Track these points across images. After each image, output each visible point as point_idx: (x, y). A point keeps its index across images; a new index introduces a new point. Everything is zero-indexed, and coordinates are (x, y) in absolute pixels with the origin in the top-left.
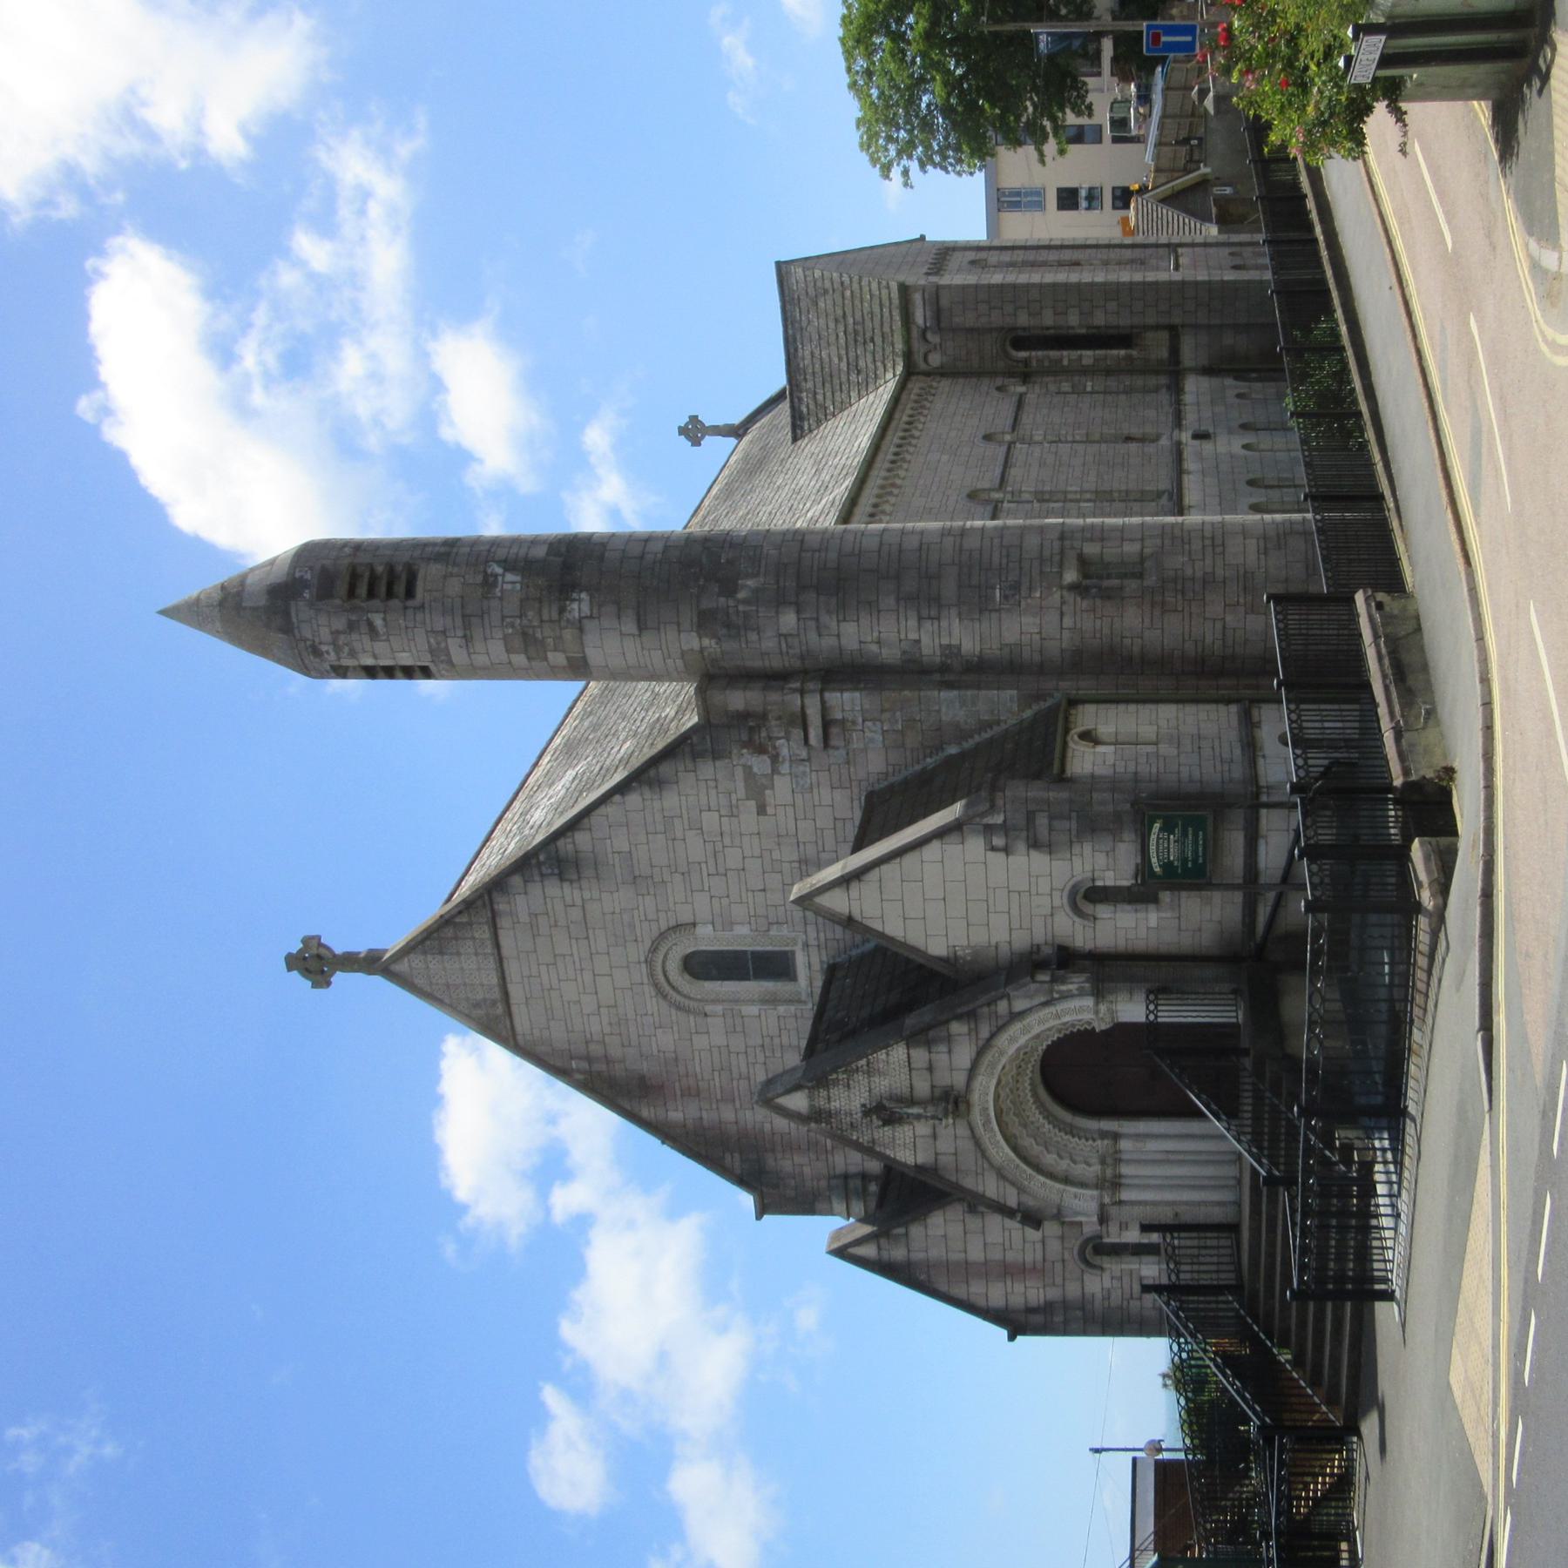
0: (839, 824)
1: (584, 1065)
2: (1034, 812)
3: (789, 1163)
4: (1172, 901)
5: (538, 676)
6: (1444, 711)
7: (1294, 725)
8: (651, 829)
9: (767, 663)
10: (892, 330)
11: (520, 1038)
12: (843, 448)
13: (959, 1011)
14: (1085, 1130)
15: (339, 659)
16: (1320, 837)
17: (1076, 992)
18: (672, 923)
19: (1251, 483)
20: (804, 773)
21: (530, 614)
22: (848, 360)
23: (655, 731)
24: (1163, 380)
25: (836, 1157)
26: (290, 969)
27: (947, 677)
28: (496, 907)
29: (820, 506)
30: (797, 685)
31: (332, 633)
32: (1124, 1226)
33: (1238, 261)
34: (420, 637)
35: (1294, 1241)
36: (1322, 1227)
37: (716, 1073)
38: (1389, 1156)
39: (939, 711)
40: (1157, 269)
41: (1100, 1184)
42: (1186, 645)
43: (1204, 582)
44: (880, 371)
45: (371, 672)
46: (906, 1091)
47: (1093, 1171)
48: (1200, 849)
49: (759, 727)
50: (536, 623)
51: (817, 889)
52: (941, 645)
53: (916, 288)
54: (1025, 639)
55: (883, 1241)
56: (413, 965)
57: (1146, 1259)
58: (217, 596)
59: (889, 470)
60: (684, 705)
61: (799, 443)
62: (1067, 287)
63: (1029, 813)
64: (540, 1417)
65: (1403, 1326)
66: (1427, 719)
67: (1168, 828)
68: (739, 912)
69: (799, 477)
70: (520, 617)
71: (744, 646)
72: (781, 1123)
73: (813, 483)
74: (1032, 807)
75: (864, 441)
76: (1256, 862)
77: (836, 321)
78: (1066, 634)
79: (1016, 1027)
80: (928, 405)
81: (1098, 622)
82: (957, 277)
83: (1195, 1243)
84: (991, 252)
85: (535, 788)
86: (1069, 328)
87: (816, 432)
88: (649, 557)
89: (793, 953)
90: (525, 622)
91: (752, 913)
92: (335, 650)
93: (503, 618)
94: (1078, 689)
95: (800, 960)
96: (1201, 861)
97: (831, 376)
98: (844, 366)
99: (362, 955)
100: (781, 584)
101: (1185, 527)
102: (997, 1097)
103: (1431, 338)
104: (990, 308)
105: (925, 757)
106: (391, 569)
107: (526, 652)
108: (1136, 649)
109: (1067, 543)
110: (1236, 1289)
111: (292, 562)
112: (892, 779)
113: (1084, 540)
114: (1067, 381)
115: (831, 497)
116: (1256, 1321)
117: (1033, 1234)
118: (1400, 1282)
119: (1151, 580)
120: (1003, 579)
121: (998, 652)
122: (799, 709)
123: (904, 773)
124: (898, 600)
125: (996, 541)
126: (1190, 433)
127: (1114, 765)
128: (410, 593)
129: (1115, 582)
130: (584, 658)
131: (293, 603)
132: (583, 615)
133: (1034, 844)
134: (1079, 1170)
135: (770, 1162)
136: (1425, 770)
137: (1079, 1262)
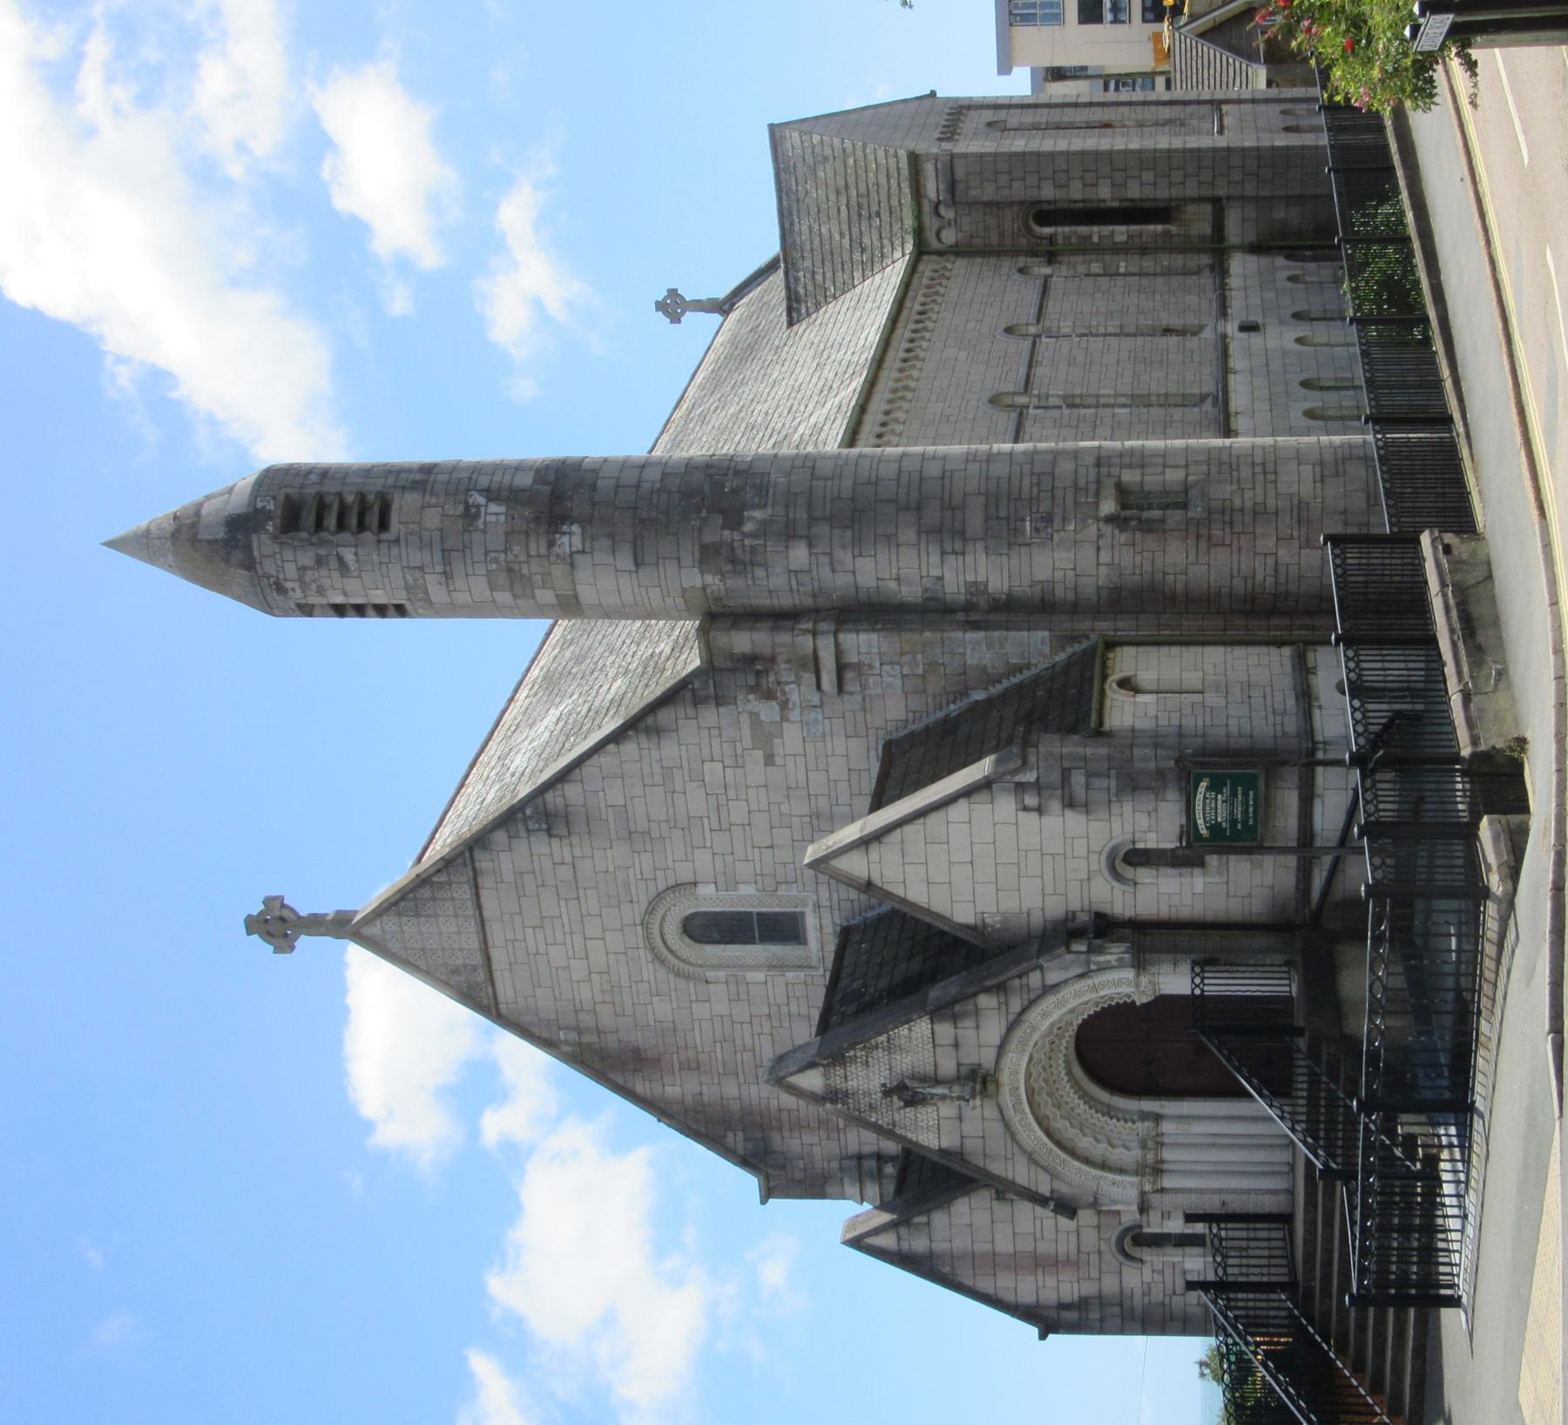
0: (854, 776)
1: (573, 1036)
2: (1069, 770)
3: (797, 1141)
4: (1220, 865)
5: (525, 615)
6: (1517, 672)
7: (1352, 675)
8: (648, 781)
9: (775, 602)
10: (900, 204)
11: (502, 1007)
12: (847, 339)
13: (988, 983)
14: (1125, 1111)
15: (306, 597)
16: (1382, 814)
17: (1115, 964)
18: (671, 882)
19: (1305, 384)
20: (816, 720)
21: (516, 548)
22: (851, 235)
23: (650, 669)
24: (1205, 260)
25: (849, 1136)
26: (249, 933)
27: (974, 617)
28: (477, 864)
29: (825, 411)
30: (809, 625)
31: (298, 569)
32: (1166, 1216)
33: (1291, 122)
34: (395, 572)
35: (1353, 1242)
36: (1385, 1229)
37: (718, 1045)
38: (1457, 1154)
39: (963, 654)
40: (1199, 132)
41: (1140, 1170)
42: (1235, 582)
43: (1255, 514)
44: (887, 250)
45: (340, 610)
46: (929, 1069)
47: (1132, 1156)
48: (1251, 810)
49: (767, 671)
50: (522, 558)
51: (834, 852)
52: (965, 582)
53: (928, 157)
54: (1059, 575)
55: (903, 1230)
56: (386, 928)
57: (1189, 1250)
58: (169, 527)
59: (901, 370)
60: (681, 641)
61: (795, 327)
62: (1097, 154)
63: (1063, 770)
64: (462, 1386)
65: (1471, 1335)
66: (1497, 680)
67: (1215, 787)
68: (743, 870)
69: (797, 371)
70: (505, 552)
71: (750, 582)
72: (788, 1100)
73: (814, 380)
74: (1066, 764)
75: (872, 335)
76: (1311, 825)
77: (838, 192)
78: (1103, 571)
79: (1049, 1001)
80: (942, 290)
81: (1138, 558)
82: (973, 143)
83: (1244, 1234)
84: (1011, 111)
85: (513, 728)
86: (1099, 201)
87: (814, 316)
88: (646, 486)
89: (803, 914)
90: (510, 557)
91: (758, 871)
92: (301, 587)
93: (486, 554)
94: (1116, 630)
95: (811, 922)
96: (1251, 822)
97: (832, 254)
98: (846, 242)
99: (329, 918)
100: (791, 516)
101: (1233, 452)
102: (1028, 1075)
103: (1506, 251)
104: (1011, 180)
105: (948, 704)
106: (362, 498)
107: (511, 589)
108: (1179, 587)
109: (1104, 470)
110: (1290, 1287)
111: (252, 491)
112: (912, 727)
113: (1122, 466)
114: (1097, 261)
115: (837, 400)
116: (1311, 1322)
117: (1064, 1222)
118: (1467, 1288)
119: (1196, 512)
120: (1034, 510)
121: (1028, 589)
122: (811, 652)
123: (926, 721)
124: (919, 533)
125: (1027, 468)
126: (1236, 325)
127: (1157, 717)
128: (384, 525)
129: (1156, 514)
130: (576, 597)
131: (254, 537)
132: (574, 549)
133: (1070, 803)
134: (1118, 1155)
135: (777, 1141)
136: (1494, 739)
137: (1117, 1254)
